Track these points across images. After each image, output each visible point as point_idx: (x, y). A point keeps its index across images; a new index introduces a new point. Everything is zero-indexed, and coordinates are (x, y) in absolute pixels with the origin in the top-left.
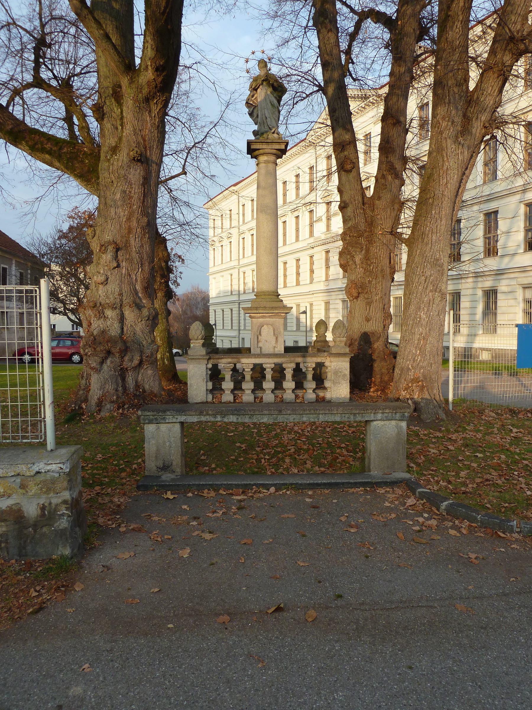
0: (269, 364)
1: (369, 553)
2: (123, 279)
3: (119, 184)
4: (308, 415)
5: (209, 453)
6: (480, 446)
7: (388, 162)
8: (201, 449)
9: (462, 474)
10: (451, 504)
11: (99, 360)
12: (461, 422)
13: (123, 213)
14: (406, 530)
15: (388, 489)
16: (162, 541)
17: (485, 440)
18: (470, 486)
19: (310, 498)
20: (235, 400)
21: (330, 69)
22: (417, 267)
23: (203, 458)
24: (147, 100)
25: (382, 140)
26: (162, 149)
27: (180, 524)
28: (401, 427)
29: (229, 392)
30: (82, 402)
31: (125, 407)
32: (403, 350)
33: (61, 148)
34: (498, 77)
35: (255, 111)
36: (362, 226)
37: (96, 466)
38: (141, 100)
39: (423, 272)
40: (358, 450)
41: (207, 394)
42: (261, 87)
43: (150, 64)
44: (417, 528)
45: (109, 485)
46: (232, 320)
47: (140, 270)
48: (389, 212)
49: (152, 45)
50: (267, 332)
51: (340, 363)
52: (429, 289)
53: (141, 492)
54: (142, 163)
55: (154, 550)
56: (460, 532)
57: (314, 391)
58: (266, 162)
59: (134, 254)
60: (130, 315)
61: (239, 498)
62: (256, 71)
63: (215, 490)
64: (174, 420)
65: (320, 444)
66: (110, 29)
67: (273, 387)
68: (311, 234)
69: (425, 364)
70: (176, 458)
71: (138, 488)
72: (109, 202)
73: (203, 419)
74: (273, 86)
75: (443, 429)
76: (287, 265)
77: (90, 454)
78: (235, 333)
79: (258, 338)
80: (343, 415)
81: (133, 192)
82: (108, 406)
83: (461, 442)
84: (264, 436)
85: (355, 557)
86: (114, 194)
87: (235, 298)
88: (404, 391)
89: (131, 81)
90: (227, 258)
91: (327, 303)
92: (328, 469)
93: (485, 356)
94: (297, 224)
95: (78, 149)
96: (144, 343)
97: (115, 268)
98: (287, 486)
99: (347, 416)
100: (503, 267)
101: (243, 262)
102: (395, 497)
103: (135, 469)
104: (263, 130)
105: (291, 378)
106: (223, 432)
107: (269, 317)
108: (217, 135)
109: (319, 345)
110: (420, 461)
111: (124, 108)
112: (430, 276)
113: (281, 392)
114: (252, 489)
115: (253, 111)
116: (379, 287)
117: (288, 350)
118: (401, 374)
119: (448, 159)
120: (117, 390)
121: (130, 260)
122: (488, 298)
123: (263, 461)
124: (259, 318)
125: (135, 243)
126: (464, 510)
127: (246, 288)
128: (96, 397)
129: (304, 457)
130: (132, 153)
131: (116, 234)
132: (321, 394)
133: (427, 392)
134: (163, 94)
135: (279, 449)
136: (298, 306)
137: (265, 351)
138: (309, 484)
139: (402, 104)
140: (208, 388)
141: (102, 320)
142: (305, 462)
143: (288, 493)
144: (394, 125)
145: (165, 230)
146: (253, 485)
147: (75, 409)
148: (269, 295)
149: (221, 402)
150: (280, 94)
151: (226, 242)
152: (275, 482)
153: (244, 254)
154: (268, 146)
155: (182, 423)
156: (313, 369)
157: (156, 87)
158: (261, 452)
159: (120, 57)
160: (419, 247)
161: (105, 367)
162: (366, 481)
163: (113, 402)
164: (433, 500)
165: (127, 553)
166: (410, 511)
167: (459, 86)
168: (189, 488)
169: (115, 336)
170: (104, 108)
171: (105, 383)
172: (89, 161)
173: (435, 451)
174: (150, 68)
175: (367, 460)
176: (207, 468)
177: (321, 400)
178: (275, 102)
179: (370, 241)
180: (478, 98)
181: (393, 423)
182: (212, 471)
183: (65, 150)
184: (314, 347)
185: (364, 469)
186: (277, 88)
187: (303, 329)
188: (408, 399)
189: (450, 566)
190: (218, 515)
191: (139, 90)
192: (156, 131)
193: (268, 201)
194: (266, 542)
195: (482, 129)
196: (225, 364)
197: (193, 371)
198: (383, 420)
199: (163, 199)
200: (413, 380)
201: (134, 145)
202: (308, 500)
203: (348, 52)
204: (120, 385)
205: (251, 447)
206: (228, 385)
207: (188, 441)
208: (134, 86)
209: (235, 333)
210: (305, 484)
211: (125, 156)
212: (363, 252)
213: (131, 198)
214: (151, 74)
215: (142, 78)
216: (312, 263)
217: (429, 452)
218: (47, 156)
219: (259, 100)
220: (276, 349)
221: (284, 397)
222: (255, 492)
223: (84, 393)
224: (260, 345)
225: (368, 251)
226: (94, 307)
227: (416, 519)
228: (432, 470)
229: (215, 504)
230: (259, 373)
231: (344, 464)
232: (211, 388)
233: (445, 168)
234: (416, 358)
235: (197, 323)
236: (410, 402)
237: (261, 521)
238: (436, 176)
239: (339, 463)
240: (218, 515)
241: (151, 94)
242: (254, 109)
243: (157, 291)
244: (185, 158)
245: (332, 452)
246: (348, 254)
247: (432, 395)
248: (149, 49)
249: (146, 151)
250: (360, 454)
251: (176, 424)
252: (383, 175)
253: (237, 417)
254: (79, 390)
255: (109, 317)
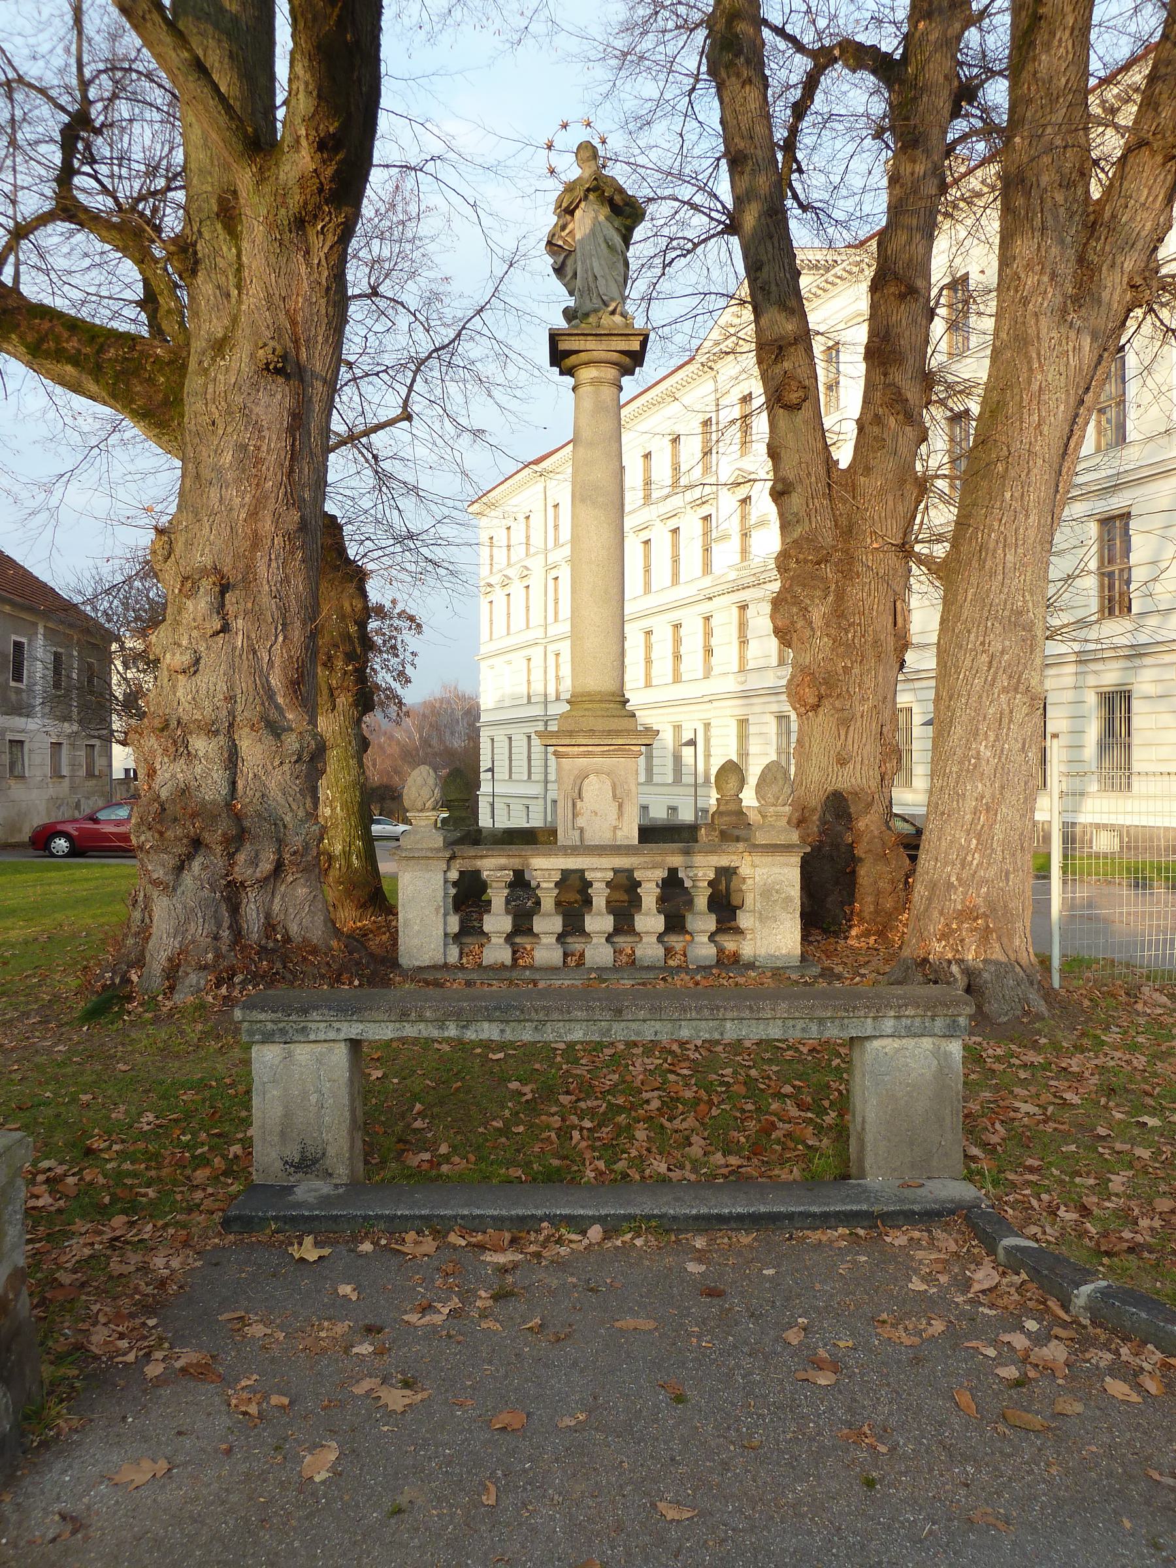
0: (599, 870)
1: (877, 1467)
2: (237, 660)
3: (230, 429)
4: (694, 1023)
5: (436, 1110)
6: (1147, 1094)
7: (887, 386)
8: (415, 1098)
9: (1117, 1182)
10: (1105, 1293)
11: (170, 861)
12: (1086, 1022)
13: (238, 499)
14: (978, 1378)
15: (916, 1234)
16: (261, 1416)
17: (1155, 1074)
18: (1144, 1223)
19: (700, 1261)
20: (515, 960)
21: (748, 169)
22: (969, 632)
23: (418, 1124)
24: (300, 223)
25: (872, 334)
26: (338, 345)
27: (324, 1350)
28: (947, 1055)
29: (502, 940)
30: (131, 966)
31: (237, 980)
32: (934, 837)
33: (101, 350)
34: (1164, 164)
35: (569, 262)
36: (828, 538)
37: (132, 1149)
38: (286, 223)
39: (983, 643)
40: (826, 1103)
41: (445, 945)
42: (583, 205)
43: (303, 132)
44: (1010, 1372)
45: (153, 1210)
46: (529, 760)
47: (281, 639)
48: (890, 503)
49: (307, 84)
50: (596, 792)
51: (776, 870)
52: (998, 684)
53: (232, 1237)
54: (288, 377)
55: (229, 1452)
56: (1139, 1387)
57: (712, 938)
58: (595, 382)
59: (266, 601)
60: (252, 749)
61: (501, 1259)
62: (571, 170)
63: (437, 1234)
64: (332, 1035)
65: (727, 1084)
66: (215, 59)
67: (611, 930)
68: (707, 567)
69: (991, 873)
70: (335, 1135)
71: (227, 1224)
72: (206, 473)
73: (410, 1031)
74: (611, 202)
75: (1043, 1041)
76: (653, 638)
77: (126, 1112)
78: (537, 789)
79: (574, 805)
80: (791, 1023)
81: (265, 448)
82: (193, 978)
83: (1095, 1080)
84: (583, 1062)
85: (834, 1486)
86: (218, 452)
87: (537, 711)
88: (939, 941)
89: (261, 178)
90: (518, 620)
91: (743, 723)
92: (749, 1159)
93: (1104, 843)
94: (675, 545)
95: (141, 352)
96: (287, 819)
97: (218, 633)
98: (636, 1224)
99: (799, 1027)
100: (1143, 639)
101: (554, 630)
102: (937, 1261)
103: (236, 1157)
104: (588, 306)
105: (653, 906)
106: (479, 1051)
107: (603, 754)
108: (485, 331)
109: (723, 822)
110: (995, 1139)
111: (245, 245)
112: (1002, 653)
113: (629, 939)
114: (538, 1231)
115: (563, 264)
116: (869, 683)
117: (650, 834)
118: (930, 899)
119: (1041, 366)
120: (216, 938)
121: (255, 615)
122: (1111, 711)
123: (576, 1134)
124: (578, 756)
125: (266, 572)
126: (1144, 1315)
127: (561, 689)
128: (163, 956)
129: (685, 1125)
130: (261, 352)
131: (220, 551)
132: (730, 945)
133: (997, 945)
134: (338, 209)
135: (620, 1101)
136: (678, 728)
137: (592, 838)
138: (697, 1218)
139: (921, 250)
140: (449, 930)
141: (182, 761)
142: (688, 1138)
143: (639, 1242)
144: (902, 297)
145: (362, 551)
146: (541, 1219)
147: (113, 983)
148: (601, 701)
149: (480, 965)
150: (628, 222)
151: (517, 589)
152: (603, 1212)
153: (556, 613)
154: (596, 343)
155: (355, 1045)
156: (711, 883)
157: (321, 190)
158: (574, 1109)
159: (231, 118)
160: (974, 580)
161: (187, 879)
162: (854, 1208)
163: (205, 968)
164: (1048, 1274)
165: (146, 1464)
166: (987, 1311)
167: (1068, 187)
168: (364, 1227)
169: (214, 802)
170: (199, 247)
171: (187, 920)
172: (168, 379)
173: (1033, 1109)
174: (304, 142)
175: (853, 1141)
176: (426, 1156)
177: (729, 962)
178: (618, 240)
179: (848, 568)
180: (1113, 216)
181: (927, 1043)
182: (439, 1164)
183: (112, 353)
184: (711, 826)
185: (845, 1173)
186: (626, 213)
187: (688, 779)
188: (949, 962)
189: (1127, 1524)
190: (438, 1319)
191: (279, 200)
192: (323, 301)
193: (600, 474)
194: (570, 1422)
195: (1124, 291)
196: (494, 868)
197: (411, 888)
198: (899, 1037)
199: (341, 467)
200: (961, 912)
201: (268, 334)
202: (693, 1268)
203: (790, 146)
204: (226, 924)
205: (548, 1093)
206: (498, 922)
207: (385, 1076)
208: (267, 189)
209: (537, 789)
210: (687, 1218)
211: (245, 359)
212: (831, 598)
213: (259, 461)
214: (308, 159)
215: (287, 168)
216: (708, 634)
217: (1016, 1110)
218: (69, 368)
219: (578, 237)
220: (619, 834)
221: (638, 953)
222: (547, 1239)
223: (136, 943)
224: (581, 822)
225: (840, 597)
226: (162, 730)
227: (1006, 1338)
228: (1031, 1170)
229: (433, 1281)
230: (574, 894)
231: (792, 1145)
232: (456, 929)
233: (1035, 387)
234: (969, 858)
235: (424, 769)
236: (955, 969)
237: (558, 1340)
238: (1011, 408)
239: (778, 1142)
240: (438, 1319)
241: (310, 208)
242: (566, 257)
243: (336, 693)
244: (408, 382)
245: (758, 1109)
246: (794, 604)
247: (1010, 953)
248: (301, 96)
249: (297, 348)
250: (833, 1114)
251: (337, 1045)
252: (876, 415)
253: (502, 1026)
254: (126, 935)
255: (201, 754)
